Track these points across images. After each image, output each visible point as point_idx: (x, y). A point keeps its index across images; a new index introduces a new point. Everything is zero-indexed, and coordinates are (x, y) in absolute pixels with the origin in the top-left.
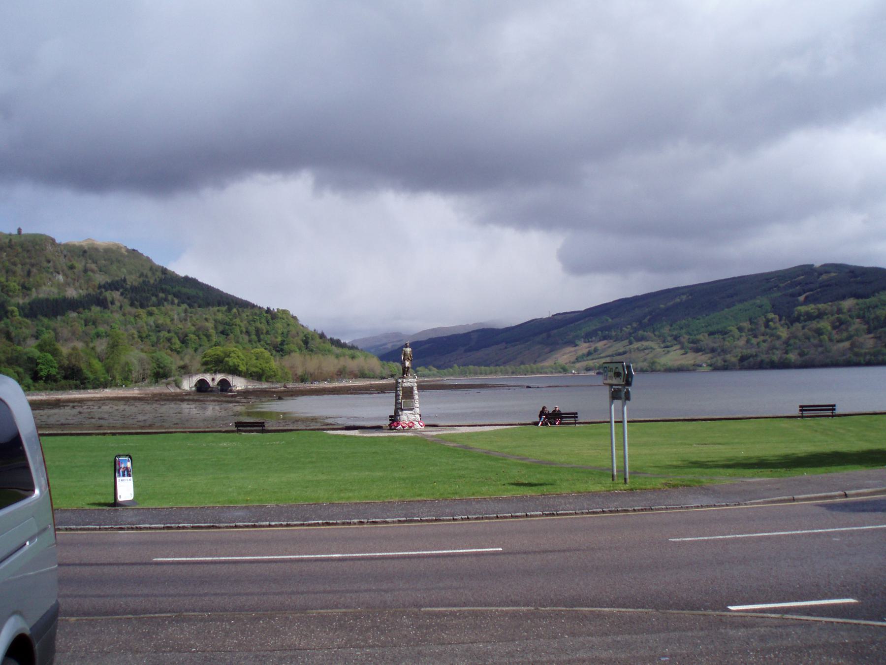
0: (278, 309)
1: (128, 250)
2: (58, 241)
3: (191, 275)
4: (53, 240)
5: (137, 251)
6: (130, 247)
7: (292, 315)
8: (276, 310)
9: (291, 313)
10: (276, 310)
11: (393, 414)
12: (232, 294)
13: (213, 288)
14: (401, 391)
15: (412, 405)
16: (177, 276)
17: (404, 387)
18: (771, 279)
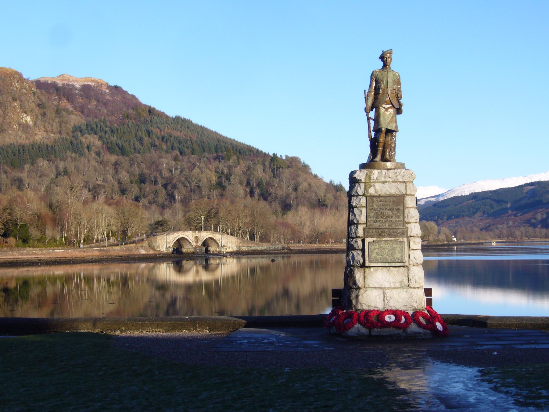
0: (286, 156)
1: (109, 87)
2: (25, 76)
3: (185, 115)
4: (20, 75)
5: (120, 88)
6: (112, 84)
7: (304, 163)
8: (284, 158)
9: (302, 161)
10: (284, 158)
11: (340, 285)
12: (232, 138)
13: (210, 130)
14: (364, 210)
15: (398, 255)
16: (122, 90)
17: (372, 196)
18: (385, 304)
